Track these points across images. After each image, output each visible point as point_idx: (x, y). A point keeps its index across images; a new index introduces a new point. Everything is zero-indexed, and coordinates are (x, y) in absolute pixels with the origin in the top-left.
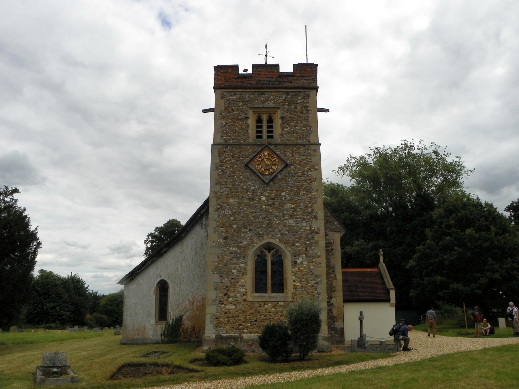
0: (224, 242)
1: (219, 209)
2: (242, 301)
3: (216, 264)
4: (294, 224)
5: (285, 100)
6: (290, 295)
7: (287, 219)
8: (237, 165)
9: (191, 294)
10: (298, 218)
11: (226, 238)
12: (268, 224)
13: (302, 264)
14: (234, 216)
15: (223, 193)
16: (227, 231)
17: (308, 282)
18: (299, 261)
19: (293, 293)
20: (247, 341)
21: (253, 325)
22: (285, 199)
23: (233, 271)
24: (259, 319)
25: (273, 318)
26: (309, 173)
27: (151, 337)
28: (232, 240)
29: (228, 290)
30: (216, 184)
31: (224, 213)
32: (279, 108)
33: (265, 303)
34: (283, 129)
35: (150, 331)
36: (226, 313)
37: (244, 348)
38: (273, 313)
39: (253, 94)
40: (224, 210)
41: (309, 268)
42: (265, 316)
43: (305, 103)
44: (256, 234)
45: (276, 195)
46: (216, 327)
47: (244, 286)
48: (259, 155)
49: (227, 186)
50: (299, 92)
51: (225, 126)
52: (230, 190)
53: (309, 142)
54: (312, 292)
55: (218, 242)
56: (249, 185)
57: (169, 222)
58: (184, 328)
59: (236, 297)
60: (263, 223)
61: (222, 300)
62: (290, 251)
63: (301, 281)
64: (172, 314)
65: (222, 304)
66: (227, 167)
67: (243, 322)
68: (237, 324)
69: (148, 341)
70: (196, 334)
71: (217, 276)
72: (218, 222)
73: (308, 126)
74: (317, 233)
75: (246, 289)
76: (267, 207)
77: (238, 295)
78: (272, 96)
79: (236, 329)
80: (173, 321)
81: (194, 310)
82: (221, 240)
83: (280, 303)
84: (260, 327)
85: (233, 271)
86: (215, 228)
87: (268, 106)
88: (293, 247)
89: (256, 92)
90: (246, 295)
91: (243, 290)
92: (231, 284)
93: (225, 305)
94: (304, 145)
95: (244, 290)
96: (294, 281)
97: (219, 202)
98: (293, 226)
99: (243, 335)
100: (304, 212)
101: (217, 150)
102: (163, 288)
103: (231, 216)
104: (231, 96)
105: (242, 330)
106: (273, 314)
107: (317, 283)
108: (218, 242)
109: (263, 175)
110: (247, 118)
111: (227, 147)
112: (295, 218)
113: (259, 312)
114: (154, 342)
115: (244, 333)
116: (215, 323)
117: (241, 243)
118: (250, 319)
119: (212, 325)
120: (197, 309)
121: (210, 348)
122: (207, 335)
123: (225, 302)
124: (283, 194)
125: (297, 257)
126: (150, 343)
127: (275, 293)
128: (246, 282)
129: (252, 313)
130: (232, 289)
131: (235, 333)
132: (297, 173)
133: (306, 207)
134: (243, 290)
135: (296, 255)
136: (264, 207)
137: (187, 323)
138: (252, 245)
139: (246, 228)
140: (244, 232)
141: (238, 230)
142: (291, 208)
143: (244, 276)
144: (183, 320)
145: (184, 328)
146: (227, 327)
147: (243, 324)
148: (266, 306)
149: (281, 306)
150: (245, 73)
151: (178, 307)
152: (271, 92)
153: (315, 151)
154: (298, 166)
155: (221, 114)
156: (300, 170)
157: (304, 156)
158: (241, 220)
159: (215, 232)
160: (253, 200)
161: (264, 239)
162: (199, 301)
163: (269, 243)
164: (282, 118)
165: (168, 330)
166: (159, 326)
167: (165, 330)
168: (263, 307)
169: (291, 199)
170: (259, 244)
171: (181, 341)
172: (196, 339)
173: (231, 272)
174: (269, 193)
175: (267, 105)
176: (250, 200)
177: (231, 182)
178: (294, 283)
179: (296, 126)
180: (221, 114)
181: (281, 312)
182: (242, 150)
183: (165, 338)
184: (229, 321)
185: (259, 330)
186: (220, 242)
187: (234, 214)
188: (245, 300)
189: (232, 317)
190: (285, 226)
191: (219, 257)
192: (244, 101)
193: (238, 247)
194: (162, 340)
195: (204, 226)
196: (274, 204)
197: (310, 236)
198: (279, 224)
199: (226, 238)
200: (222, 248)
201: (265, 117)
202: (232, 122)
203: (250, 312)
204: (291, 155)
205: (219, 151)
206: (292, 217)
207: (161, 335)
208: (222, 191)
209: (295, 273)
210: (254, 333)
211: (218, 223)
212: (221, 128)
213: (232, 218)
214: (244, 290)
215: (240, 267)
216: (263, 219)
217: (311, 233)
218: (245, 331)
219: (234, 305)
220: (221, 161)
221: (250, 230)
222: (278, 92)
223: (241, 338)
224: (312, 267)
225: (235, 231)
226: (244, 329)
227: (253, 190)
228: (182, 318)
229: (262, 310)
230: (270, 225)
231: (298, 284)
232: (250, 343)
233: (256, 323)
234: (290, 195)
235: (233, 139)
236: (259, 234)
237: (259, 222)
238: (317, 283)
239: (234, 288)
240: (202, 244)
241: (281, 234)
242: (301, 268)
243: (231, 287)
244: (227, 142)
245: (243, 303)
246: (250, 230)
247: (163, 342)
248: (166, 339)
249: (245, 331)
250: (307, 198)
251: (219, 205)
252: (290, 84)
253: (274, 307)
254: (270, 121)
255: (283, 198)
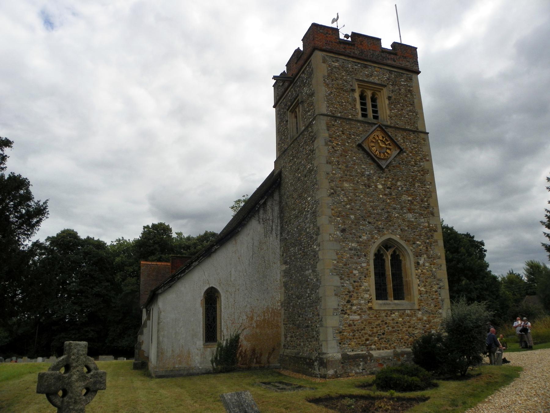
0: (342, 236)
1: (333, 194)
2: (367, 310)
3: (335, 262)
4: (413, 220)
5: (388, 79)
6: (416, 302)
7: (405, 213)
8: (348, 143)
9: (249, 306)
10: (416, 213)
11: (343, 231)
12: (387, 217)
13: (424, 265)
14: (350, 204)
15: (335, 174)
16: (344, 222)
17: (432, 287)
18: (421, 262)
19: (419, 300)
20: (377, 360)
21: (382, 339)
22: (402, 189)
23: (355, 272)
24: (387, 332)
25: (401, 330)
26: (422, 164)
27: (198, 365)
28: (351, 234)
29: (351, 297)
30: (327, 163)
31: (339, 200)
32: (385, 86)
33: (392, 311)
34: (391, 111)
35: (197, 357)
36: (350, 325)
37: (374, 369)
38: (401, 323)
39: (356, 65)
40: (339, 195)
41: (431, 271)
42: (393, 328)
43: (409, 86)
44: (376, 228)
45: (392, 184)
46: (340, 343)
47: (368, 290)
48: (372, 136)
49: (340, 166)
50: (402, 73)
51: (330, 95)
52: (344, 172)
53: (418, 129)
54: (437, 299)
55: (334, 234)
56: (363, 168)
57: (63, 232)
58: (241, 351)
59: (360, 304)
60: (381, 215)
61: (345, 308)
62: (411, 250)
63: (425, 286)
64: (225, 332)
65: (345, 313)
66: (337, 144)
67: (370, 336)
68: (364, 339)
69: (194, 371)
70: (256, 358)
71: (337, 278)
72: (332, 210)
73: (414, 112)
74: (435, 231)
75: (370, 295)
76: (385, 197)
77: (362, 302)
78: (376, 71)
79: (363, 345)
80: (227, 342)
81: (253, 327)
82: (338, 232)
83: (407, 311)
84: (389, 341)
85: (355, 272)
86: (330, 217)
87: (373, 81)
88: (414, 246)
89: (359, 63)
90: (371, 302)
91: (367, 296)
92: (354, 288)
93: (349, 315)
94: (414, 132)
95: (368, 296)
96: (419, 285)
97: (332, 185)
98: (412, 221)
99: (371, 352)
100: (421, 207)
101: (325, 122)
102: (211, 298)
103: (347, 204)
104: (333, 62)
105: (369, 347)
106: (400, 325)
107: (440, 288)
108: (334, 234)
109: (379, 158)
110: (353, 90)
111: (336, 121)
112: (414, 212)
113: (386, 323)
114: (203, 371)
115: (372, 350)
116: (339, 338)
117: (360, 237)
118: (377, 332)
119: (335, 341)
120: (257, 326)
121: (336, 372)
122: (331, 355)
123: (348, 311)
124: (399, 183)
125: (419, 257)
126: (198, 374)
127: (398, 299)
128: (369, 286)
129: (379, 325)
130: (355, 294)
131: (362, 351)
132: (410, 162)
133: (422, 201)
134: (367, 296)
135: (418, 255)
136: (381, 196)
137: (245, 344)
138: (373, 241)
139: (365, 220)
140: (363, 225)
141: (356, 221)
142: (409, 201)
143: (367, 279)
144: (240, 340)
145: (241, 351)
146: (353, 343)
147: (370, 338)
148: (393, 315)
149: (408, 315)
150: (345, 39)
151: (233, 323)
152: (375, 67)
153: (424, 140)
154: (411, 154)
155: (324, 80)
156: (412, 159)
157: (414, 143)
158: (358, 210)
159: (330, 222)
160: (369, 187)
161: (385, 234)
162: (259, 316)
163: (390, 239)
164: (389, 98)
165: (221, 355)
166: (209, 349)
167: (217, 355)
168: (390, 316)
169: (408, 190)
170: (380, 240)
171: (240, 368)
172: (258, 365)
173: (352, 273)
174: (385, 181)
175: (371, 79)
176: (366, 187)
177: (344, 162)
178: (419, 288)
179: (402, 110)
180: (324, 80)
181: (409, 322)
182: (352, 126)
183: (217, 365)
184: (354, 335)
185: (388, 345)
186: (336, 234)
187: (350, 202)
188: (370, 308)
189: (358, 330)
190: (404, 220)
191: (337, 254)
192: (347, 71)
193: (358, 242)
194: (214, 369)
195: (261, 220)
196: (391, 194)
197: (429, 234)
198: (398, 217)
199: (343, 231)
200: (340, 242)
201: (369, 94)
202: (338, 93)
203: (377, 323)
204: (402, 141)
205: (327, 124)
206: (410, 210)
207: (212, 362)
208: (334, 172)
209: (419, 276)
210: (383, 350)
211: (333, 212)
212: (326, 96)
213: (348, 206)
214: (368, 296)
215: (362, 267)
216: (381, 210)
217: (430, 231)
218: (373, 347)
219: (359, 315)
220: (330, 136)
221: (369, 223)
222: (381, 68)
223: (371, 356)
224: (434, 269)
225: (353, 222)
226: (371, 345)
227: (368, 175)
228: (239, 338)
229: (389, 320)
230: (389, 219)
231: (423, 289)
232: (381, 362)
233: (384, 336)
234: (406, 185)
235: (340, 112)
236: (379, 228)
237: (378, 214)
238: (440, 288)
239: (357, 293)
240: (260, 243)
241: (401, 230)
242: (424, 271)
243: (353, 292)
244: (333, 113)
245: (368, 312)
246: (369, 223)
247: (215, 372)
248: (219, 367)
249: (373, 347)
250: (422, 190)
251: (333, 189)
252: (393, 63)
253: (400, 316)
254: (374, 100)
255: (400, 189)
